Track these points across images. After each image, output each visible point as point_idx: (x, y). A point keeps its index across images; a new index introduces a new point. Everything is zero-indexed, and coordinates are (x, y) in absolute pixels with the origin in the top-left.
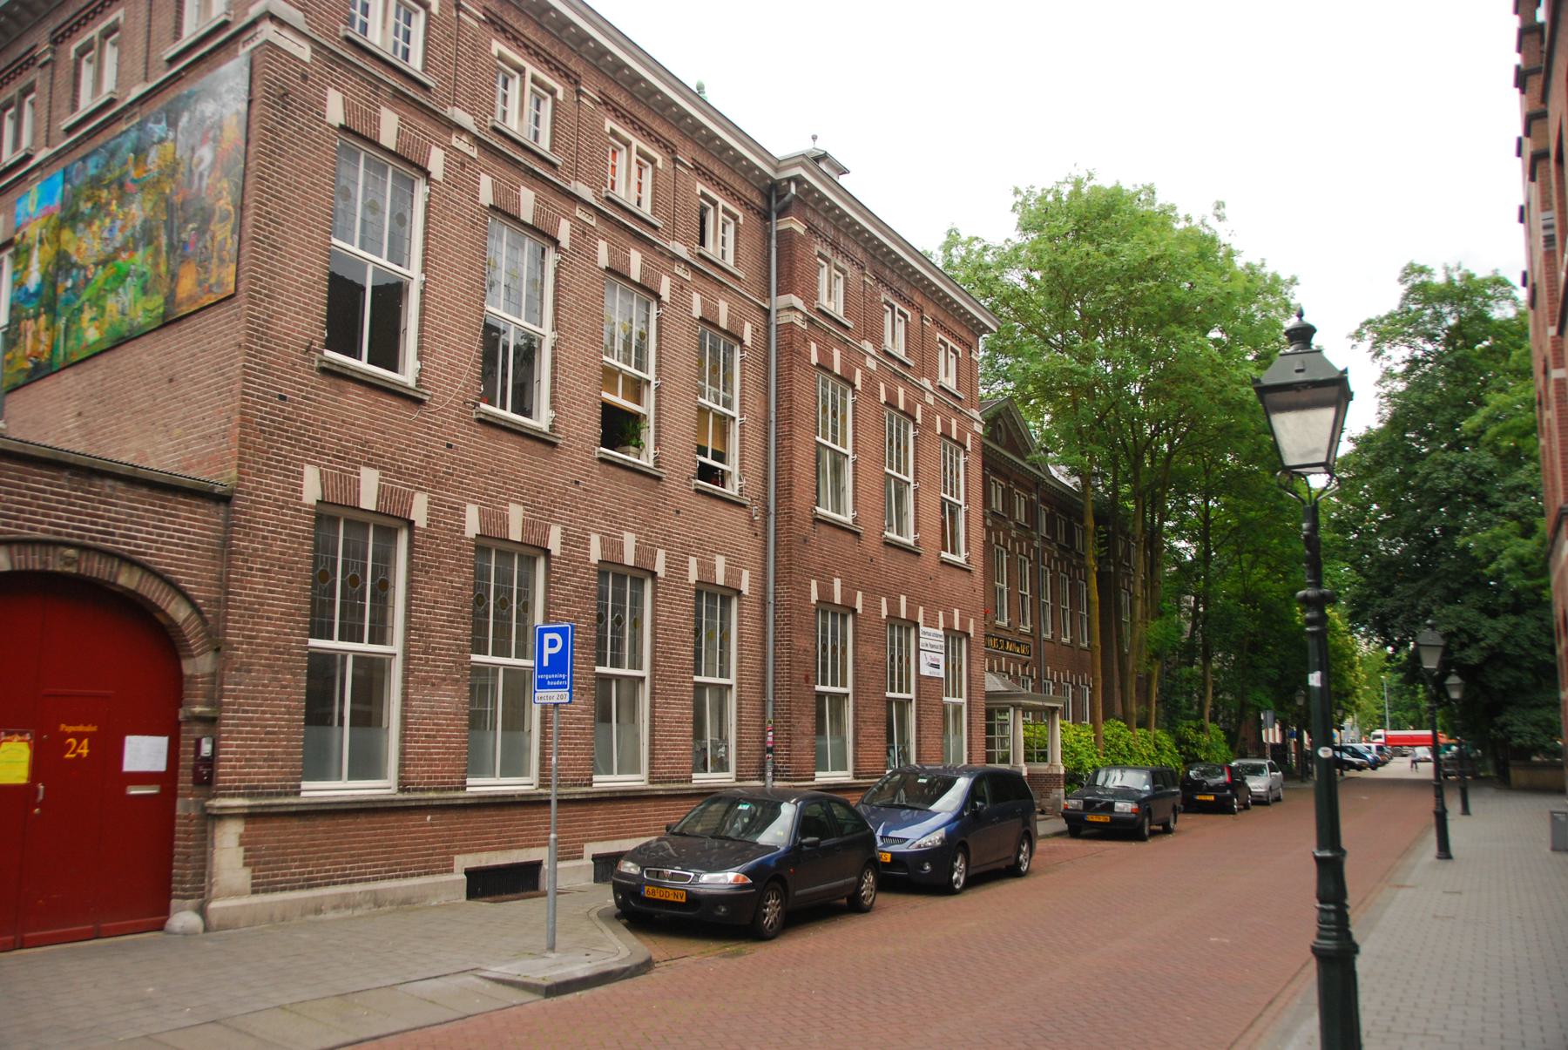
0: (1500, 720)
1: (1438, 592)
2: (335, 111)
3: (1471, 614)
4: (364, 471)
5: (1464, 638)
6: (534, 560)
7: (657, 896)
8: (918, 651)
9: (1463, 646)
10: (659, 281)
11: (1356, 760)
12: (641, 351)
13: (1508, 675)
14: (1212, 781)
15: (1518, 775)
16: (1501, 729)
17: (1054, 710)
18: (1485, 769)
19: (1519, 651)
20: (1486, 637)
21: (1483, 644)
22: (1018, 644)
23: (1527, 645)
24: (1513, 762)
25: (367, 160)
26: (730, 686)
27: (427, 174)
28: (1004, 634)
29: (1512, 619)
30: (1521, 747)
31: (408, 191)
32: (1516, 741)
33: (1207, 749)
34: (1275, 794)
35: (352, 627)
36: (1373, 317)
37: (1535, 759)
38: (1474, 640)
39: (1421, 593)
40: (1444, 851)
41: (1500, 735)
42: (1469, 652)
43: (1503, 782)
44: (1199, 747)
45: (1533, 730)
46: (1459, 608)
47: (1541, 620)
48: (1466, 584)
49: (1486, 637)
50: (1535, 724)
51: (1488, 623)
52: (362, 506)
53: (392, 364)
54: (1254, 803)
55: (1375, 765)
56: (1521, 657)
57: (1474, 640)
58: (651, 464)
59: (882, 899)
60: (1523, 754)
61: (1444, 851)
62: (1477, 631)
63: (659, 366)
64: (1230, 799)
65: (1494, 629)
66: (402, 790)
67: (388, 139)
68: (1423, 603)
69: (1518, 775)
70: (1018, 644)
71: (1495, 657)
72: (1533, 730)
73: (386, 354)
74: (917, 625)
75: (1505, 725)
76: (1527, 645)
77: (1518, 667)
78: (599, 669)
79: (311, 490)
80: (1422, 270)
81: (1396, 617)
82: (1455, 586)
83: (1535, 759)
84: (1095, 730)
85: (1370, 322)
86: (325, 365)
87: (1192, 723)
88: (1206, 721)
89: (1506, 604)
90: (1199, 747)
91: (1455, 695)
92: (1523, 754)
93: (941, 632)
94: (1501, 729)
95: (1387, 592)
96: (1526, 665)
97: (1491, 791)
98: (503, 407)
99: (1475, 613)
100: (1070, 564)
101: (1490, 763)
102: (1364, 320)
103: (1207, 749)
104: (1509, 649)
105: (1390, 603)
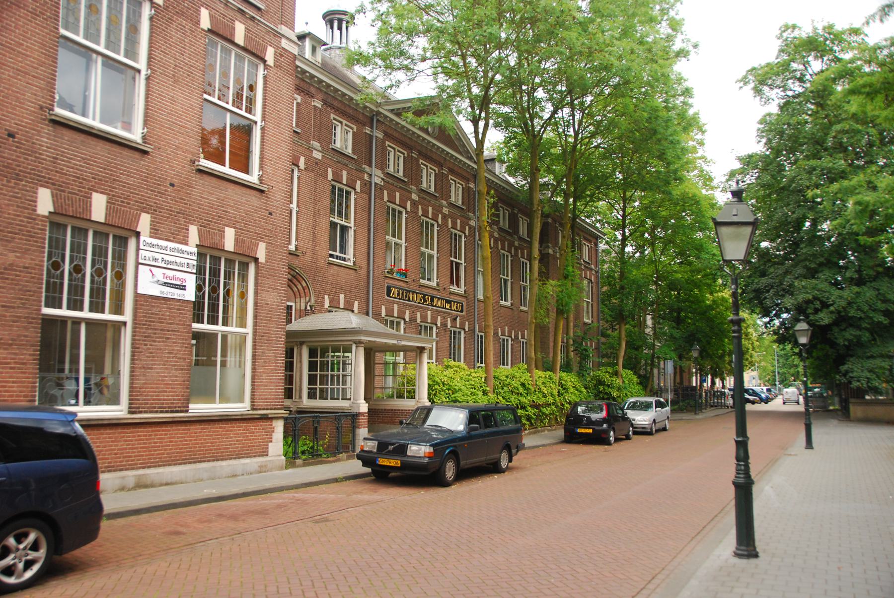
0: (843, 368)
1: (800, 270)
2: (205, 22)
3: (824, 286)
4: (227, 229)
5: (818, 304)
6: (247, 264)
7: (392, 464)
8: (138, 264)
9: (817, 311)
10: (265, 50)
11: (751, 398)
12: (251, 101)
13: (850, 334)
14: (595, 416)
15: (855, 410)
16: (845, 375)
17: (421, 350)
18: (833, 404)
19: (860, 314)
20: (834, 303)
21: (832, 308)
22: (448, 302)
23: (866, 308)
24: (852, 400)
25: (222, 46)
26: (125, 323)
27: (264, 61)
28: (434, 293)
29: (856, 289)
30: (858, 388)
31: (255, 72)
32: (855, 384)
33: (619, 389)
34: (659, 426)
35: (75, 301)
36: (756, 66)
37: (867, 397)
38: (825, 305)
39: (787, 272)
40: (809, 444)
41: (844, 380)
42: (821, 315)
43: (844, 414)
44: (613, 387)
45: (868, 375)
46: (814, 281)
47: (878, 290)
48: (821, 265)
49: (834, 303)
50: (870, 371)
51: (836, 293)
52: (94, 218)
53: (246, 171)
54: (635, 433)
55: (767, 401)
56: (861, 318)
57: (825, 305)
58: (140, 141)
59: (635, 437)
60: (859, 394)
61: (809, 444)
62: (828, 298)
63: (150, 58)
64: (606, 432)
65: (841, 297)
66: (130, 412)
67: (240, 39)
68: (788, 279)
69: (855, 410)
70: (448, 302)
71: (842, 320)
72: (868, 375)
73: (242, 162)
74: (138, 234)
75: (847, 372)
76: (866, 308)
77: (859, 328)
78: (196, 326)
79: (45, 202)
80: (794, 27)
81: (768, 291)
82: (813, 266)
83: (867, 397)
84: (487, 371)
85: (754, 69)
86: (53, 118)
87: (610, 369)
88: (620, 368)
89: (852, 279)
90: (613, 387)
91: (803, 340)
92: (859, 394)
93: (195, 250)
94: (845, 375)
95: (763, 274)
96: (865, 325)
97: (835, 422)
98: (94, 119)
99: (827, 284)
100: (511, 245)
101: (836, 399)
102: (749, 68)
103: (619, 389)
104: (852, 313)
105: (764, 281)
